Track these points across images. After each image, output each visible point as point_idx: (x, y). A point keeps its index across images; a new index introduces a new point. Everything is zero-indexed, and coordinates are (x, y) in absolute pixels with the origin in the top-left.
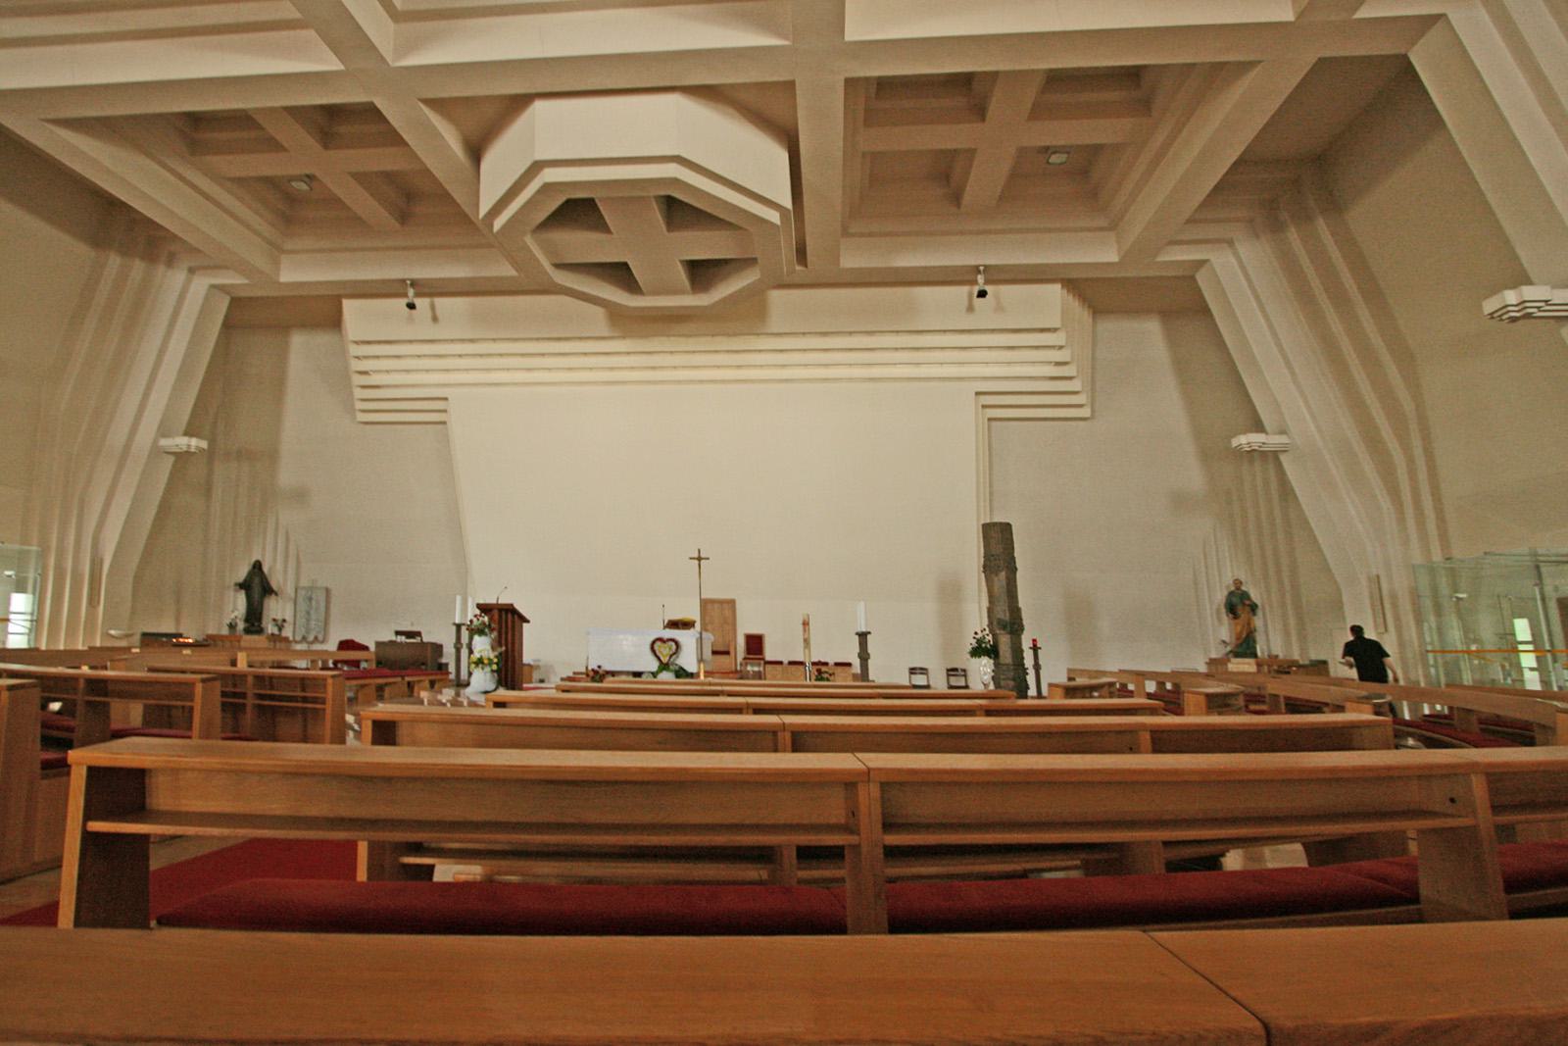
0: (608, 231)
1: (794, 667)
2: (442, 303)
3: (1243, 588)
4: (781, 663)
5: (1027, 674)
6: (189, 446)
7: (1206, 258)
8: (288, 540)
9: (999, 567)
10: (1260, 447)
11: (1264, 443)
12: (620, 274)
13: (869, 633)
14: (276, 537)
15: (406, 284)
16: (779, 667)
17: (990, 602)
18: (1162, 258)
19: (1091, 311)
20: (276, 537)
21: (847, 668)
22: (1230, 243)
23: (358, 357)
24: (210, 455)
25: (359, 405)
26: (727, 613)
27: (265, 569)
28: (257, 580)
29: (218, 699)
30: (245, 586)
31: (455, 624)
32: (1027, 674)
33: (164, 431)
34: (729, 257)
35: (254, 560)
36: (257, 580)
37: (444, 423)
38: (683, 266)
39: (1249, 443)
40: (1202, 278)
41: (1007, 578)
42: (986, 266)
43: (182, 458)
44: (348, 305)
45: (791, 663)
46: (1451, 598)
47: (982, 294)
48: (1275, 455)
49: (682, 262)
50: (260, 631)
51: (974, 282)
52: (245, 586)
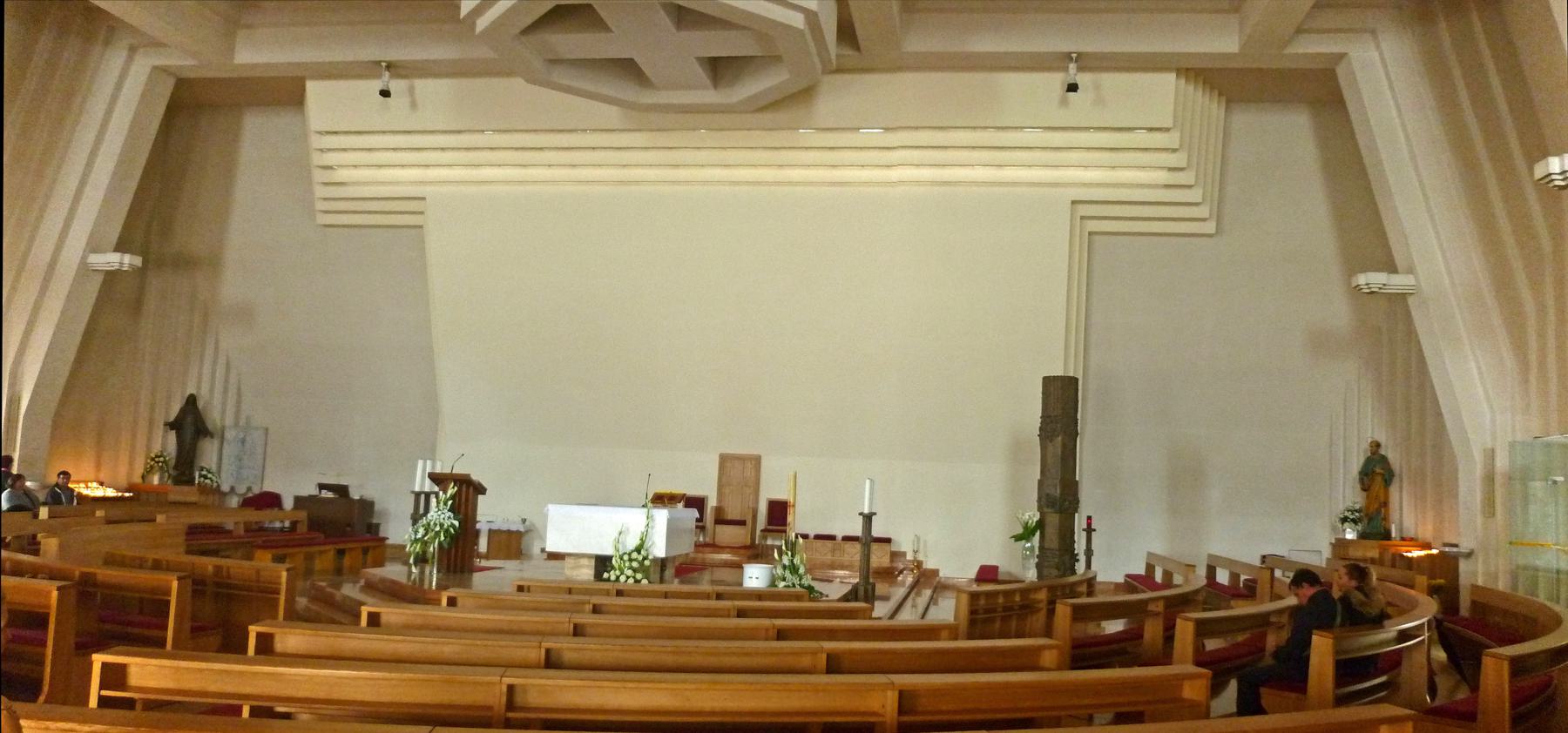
0: (607, 29)
1: (820, 542)
2: (421, 84)
3: (1383, 452)
4: (832, 538)
5: (1078, 560)
6: (122, 264)
7: (1343, 51)
8: (217, 348)
9: (1055, 430)
10: (1380, 288)
11: (1384, 285)
12: (628, 69)
13: (875, 514)
14: (215, 362)
15: (381, 66)
16: (829, 543)
17: (1042, 472)
18: (1290, 50)
19: (1224, 99)
20: (215, 362)
21: (884, 546)
22: (1373, 32)
23: (320, 133)
24: (141, 273)
25: (320, 206)
26: (749, 472)
27: (200, 404)
28: (189, 419)
29: (189, 589)
30: (176, 425)
31: (413, 492)
32: (1078, 560)
33: (94, 247)
34: (751, 54)
35: (188, 393)
36: (189, 419)
37: (421, 227)
38: (701, 65)
39: (1367, 284)
40: (1341, 71)
41: (1064, 446)
42: (1080, 55)
43: (111, 277)
44: (311, 86)
45: (818, 537)
46: (1547, 481)
47: (1073, 88)
48: (1402, 297)
49: (698, 59)
50: (191, 482)
51: (1066, 69)
52: (176, 425)
